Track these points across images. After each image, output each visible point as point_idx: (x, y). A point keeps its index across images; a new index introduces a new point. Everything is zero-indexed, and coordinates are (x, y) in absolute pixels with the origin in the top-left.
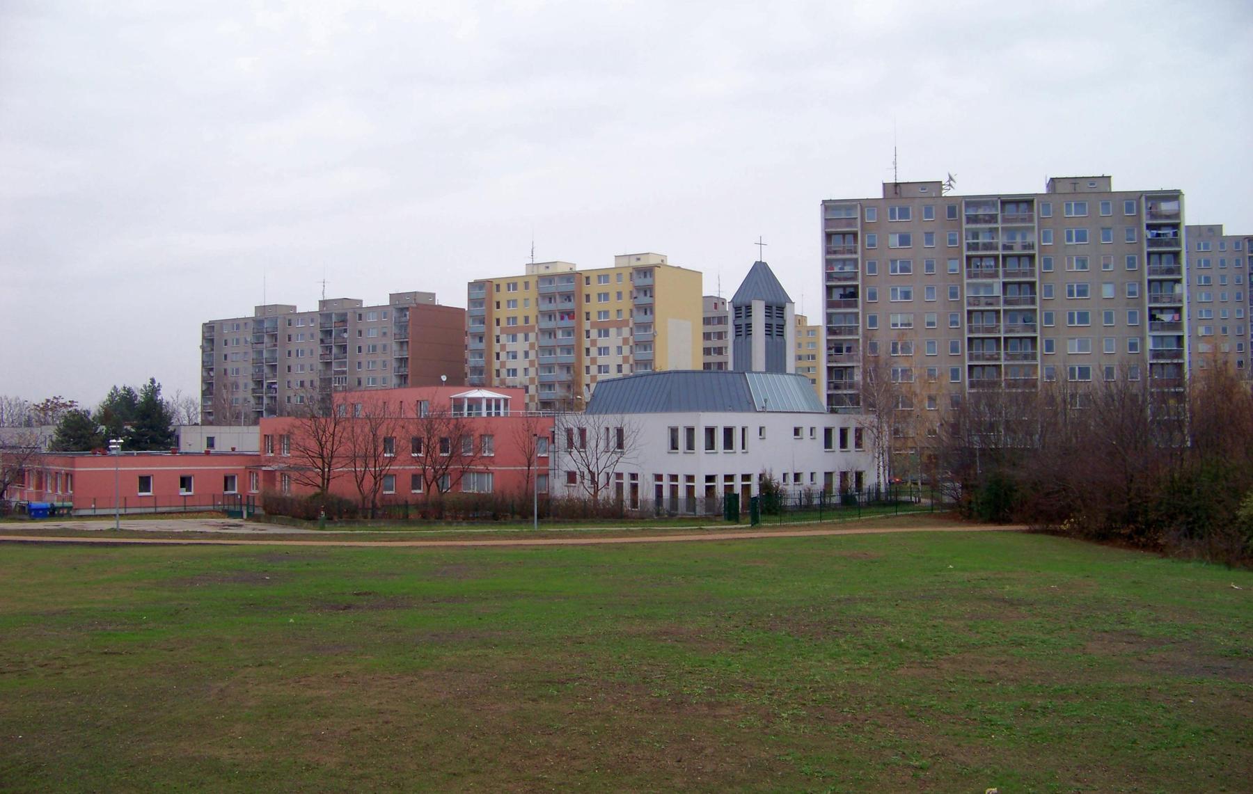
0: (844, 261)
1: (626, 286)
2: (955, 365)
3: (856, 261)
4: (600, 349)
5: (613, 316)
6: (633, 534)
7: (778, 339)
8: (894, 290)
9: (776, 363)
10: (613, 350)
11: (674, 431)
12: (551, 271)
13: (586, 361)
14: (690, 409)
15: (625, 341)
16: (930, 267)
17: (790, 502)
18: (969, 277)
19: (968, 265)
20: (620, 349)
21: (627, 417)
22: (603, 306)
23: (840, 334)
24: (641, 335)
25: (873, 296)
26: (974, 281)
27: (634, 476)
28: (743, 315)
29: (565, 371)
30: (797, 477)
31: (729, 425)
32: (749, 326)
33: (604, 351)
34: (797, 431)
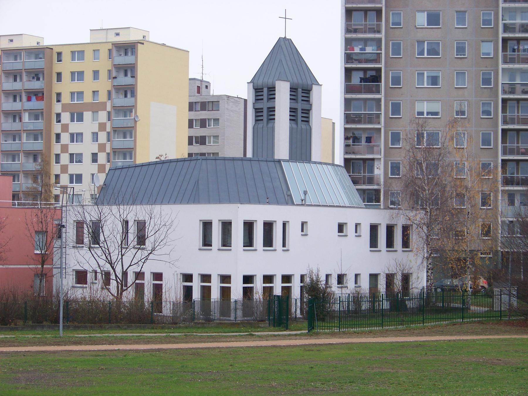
0: (366, 41)
1: (104, 65)
2: (485, 159)
3: (379, 40)
4: (72, 135)
5: (88, 98)
6: (175, 340)
7: (304, 126)
8: (421, 75)
9: (301, 150)
10: (87, 137)
11: (207, 226)
12: (16, 45)
13: (56, 148)
14: (230, 201)
15: (102, 127)
16: (461, 49)
17: (336, 307)
18: (505, 62)
19: (504, 49)
20: (95, 136)
21: (157, 208)
22: (77, 86)
23: (359, 122)
24: (120, 120)
25: (396, 80)
26: (511, 66)
27: (158, 276)
28: (265, 97)
29: (31, 160)
30: (341, 278)
31: (269, 219)
32: (272, 110)
33: (76, 137)
34: (341, 228)
